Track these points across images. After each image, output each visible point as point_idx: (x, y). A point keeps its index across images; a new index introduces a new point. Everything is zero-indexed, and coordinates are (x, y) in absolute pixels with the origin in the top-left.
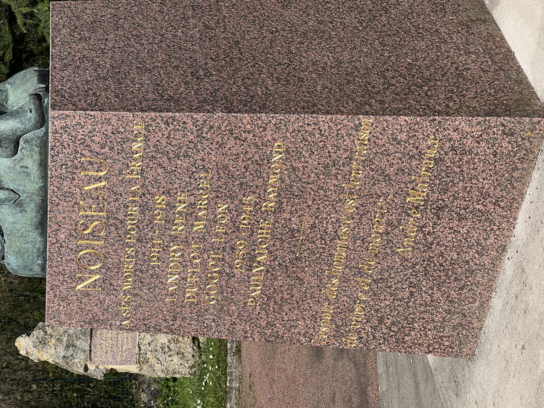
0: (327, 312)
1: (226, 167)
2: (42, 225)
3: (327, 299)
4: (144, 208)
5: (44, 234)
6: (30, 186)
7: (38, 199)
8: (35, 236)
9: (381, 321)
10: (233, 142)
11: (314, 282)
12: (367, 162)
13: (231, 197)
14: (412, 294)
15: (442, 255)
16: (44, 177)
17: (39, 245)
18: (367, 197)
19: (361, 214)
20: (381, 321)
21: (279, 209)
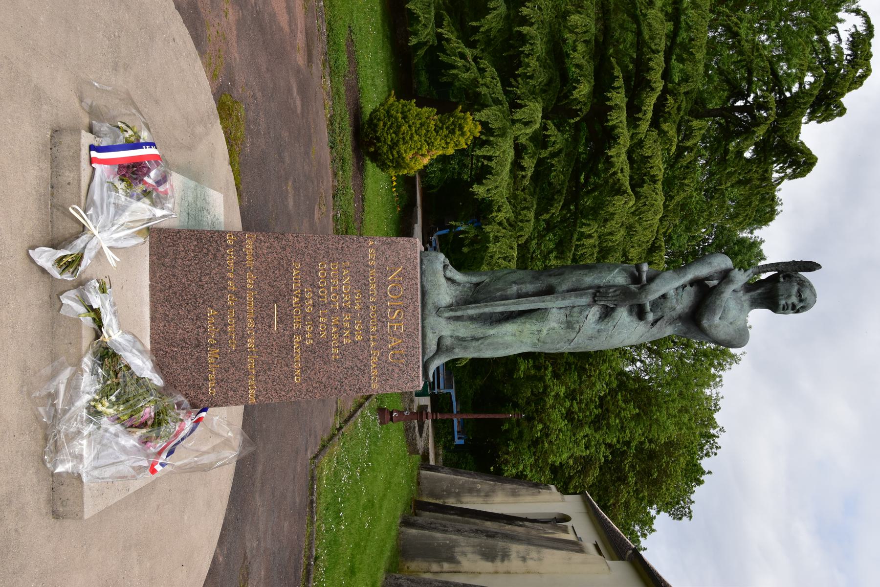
0: (250, 262)
1: (325, 363)
2: (424, 294)
3: (252, 271)
4: (367, 331)
5: (423, 287)
6: (432, 320)
7: (427, 312)
9: (215, 256)
10: (323, 380)
11: (262, 284)
12: (247, 374)
13: (319, 343)
14: (201, 280)
15: (189, 312)
16: (423, 327)
18: (242, 350)
19: (243, 338)
20: (215, 256)
21: (291, 337)
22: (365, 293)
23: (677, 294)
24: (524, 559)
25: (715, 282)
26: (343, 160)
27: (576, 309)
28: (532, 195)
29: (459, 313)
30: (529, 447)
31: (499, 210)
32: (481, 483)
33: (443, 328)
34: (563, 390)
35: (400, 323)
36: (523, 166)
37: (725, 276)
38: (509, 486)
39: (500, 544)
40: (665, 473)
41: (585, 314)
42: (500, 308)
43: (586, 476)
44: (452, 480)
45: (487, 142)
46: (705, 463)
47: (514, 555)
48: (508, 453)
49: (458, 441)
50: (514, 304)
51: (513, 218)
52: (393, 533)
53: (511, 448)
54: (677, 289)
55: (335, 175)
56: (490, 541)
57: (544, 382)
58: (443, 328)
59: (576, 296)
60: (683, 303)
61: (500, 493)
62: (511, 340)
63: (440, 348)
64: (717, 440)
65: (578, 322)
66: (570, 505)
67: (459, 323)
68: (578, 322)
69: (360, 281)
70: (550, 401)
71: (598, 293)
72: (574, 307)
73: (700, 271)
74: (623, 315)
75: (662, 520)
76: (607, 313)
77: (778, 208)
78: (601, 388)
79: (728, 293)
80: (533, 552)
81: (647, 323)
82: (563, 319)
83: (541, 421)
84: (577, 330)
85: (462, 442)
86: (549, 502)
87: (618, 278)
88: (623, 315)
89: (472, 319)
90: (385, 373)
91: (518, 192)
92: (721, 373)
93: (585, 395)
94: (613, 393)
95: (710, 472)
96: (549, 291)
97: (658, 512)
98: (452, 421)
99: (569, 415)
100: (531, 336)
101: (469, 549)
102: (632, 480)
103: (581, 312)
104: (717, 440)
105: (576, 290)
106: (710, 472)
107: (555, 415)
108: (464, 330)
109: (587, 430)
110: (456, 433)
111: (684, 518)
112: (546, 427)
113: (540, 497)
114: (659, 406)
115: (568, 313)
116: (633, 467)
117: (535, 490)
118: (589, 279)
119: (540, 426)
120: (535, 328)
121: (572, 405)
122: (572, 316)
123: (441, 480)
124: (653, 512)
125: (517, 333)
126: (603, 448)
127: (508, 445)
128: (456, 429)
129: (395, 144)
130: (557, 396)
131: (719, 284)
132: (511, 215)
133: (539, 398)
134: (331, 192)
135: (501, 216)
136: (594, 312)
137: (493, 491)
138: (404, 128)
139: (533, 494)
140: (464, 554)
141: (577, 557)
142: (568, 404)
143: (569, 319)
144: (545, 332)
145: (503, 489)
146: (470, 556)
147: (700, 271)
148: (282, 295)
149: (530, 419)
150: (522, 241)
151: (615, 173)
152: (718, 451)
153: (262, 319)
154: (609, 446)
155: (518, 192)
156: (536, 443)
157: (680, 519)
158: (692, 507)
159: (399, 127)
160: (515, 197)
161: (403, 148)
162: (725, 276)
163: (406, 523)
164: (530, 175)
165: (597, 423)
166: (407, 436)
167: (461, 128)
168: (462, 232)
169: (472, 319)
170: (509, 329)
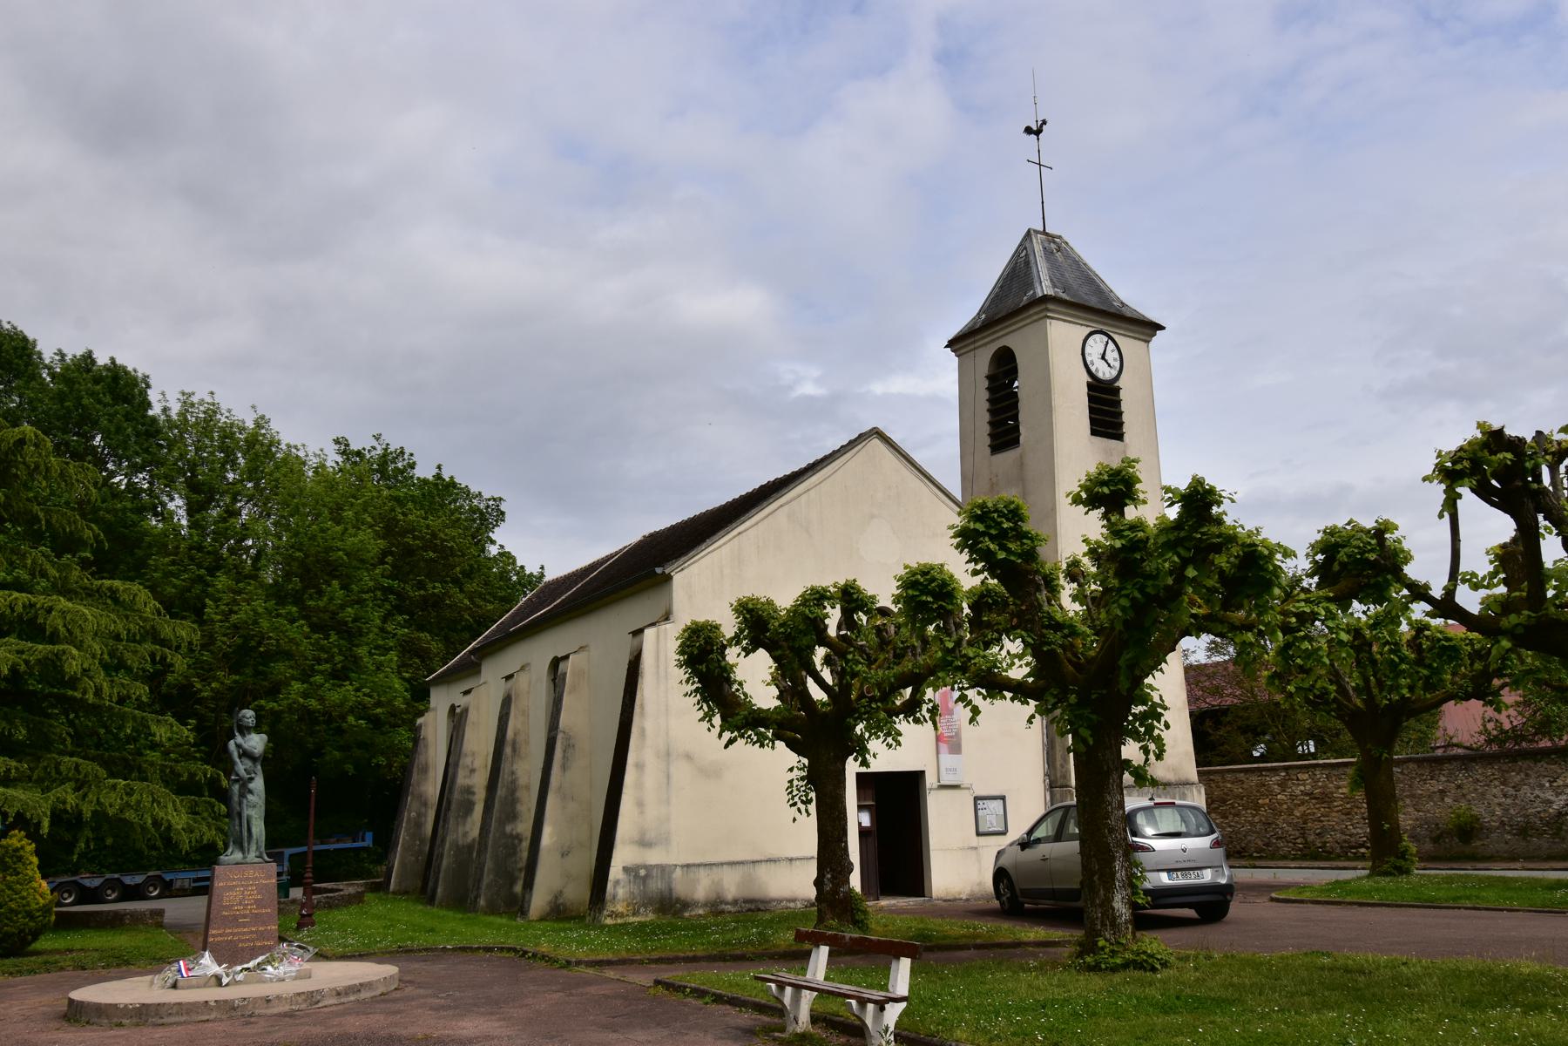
24: (473, 771)
26: (46, 963)
28: (39, 759)
30: (383, 734)
31: (64, 802)
32: (410, 811)
33: (252, 856)
34: (296, 686)
35: (250, 873)
37: (238, 746)
38: (415, 776)
39: (456, 796)
40: (432, 542)
42: (245, 834)
43: (427, 651)
44: (405, 849)
46: (424, 471)
47: (468, 782)
48: (390, 766)
49: (368, 842)
51: (72, 784)
52: (443, 912)
53: (382, 761)
55: (62, 969)
56: (453, 806)
57: (282, 712)
58: (252, 856)
60: (249, 763)
61: (423, 788)
62: (258, 828)
63: (260, 856)
64: (392, 449)
66: (441, 700)
69: (232, 888)
70: (313, 704)
71: (242, 795)
73: (235, 755)
74: (251, 786)
75: (503, 538)
76: (251, 792)
78: (298, 631)
79: (246, 746)
80: (466, 761)
83: (343, 717)
85: (369, 836)
86: (434, 725)
87: (236, 788)
88: (251, 786)
90: (269, 877)
91: (35, 777)
92: (283, 446)
93: (308, 654)
94: (306, 613)
95: (439, 467)
96: (240, 815)
97: (493, 542)
98: (315, 852)
99: (339, 676)
101: (461, 829)
102: (438, 588)
104: (392, 449)
105: (240, 804)
106: (439, 467)
107: (334, 697)
108: (253, 847)
109: (362, 651)
110: (355, 845)
111: (502, 508)
112: (351, 711)
113: (430, 738)
114: (329, 549)
116: (421, 585)
117: (421, 744)
118: (236, 799)
119: (351, 719)
121: (322, 672)
123: (402, 864)
124: (493, 550)
126: (390, 627)
127: (378, 765)
128: (349, 845)
129: (30, 915)
130: (305, 695)
132: (69, 786)
133: (307, 715)
134: (80, 972)
135: (71, 799)
136: (250, 797)
137: (421, 796)
138: (13, 905)
139: (426, 746)
140: (465, 834)
141: (472, 716)
142: (318, 679)
145: (419, 784)
146: (468, 828)
147: (235, 755)
148: (236, 918)
149: (340, 731)
150: (103, 773)
151: (27, 662)
152: (407, 451)
153: (244, 925)
154: (385, 619)
155: (35, 777)
156: (376, 722)
157: (503, 513)
158: (486, 495)
159: (11, 910)
160: (40, 781)
161: (34, 906)
162: (238, 746)
163: (431, 900)
164: (14, 764)
165: (351, 634)
166: (337, 906)
167: (17, 850)
168: (88, 846)
170: (254, 830)
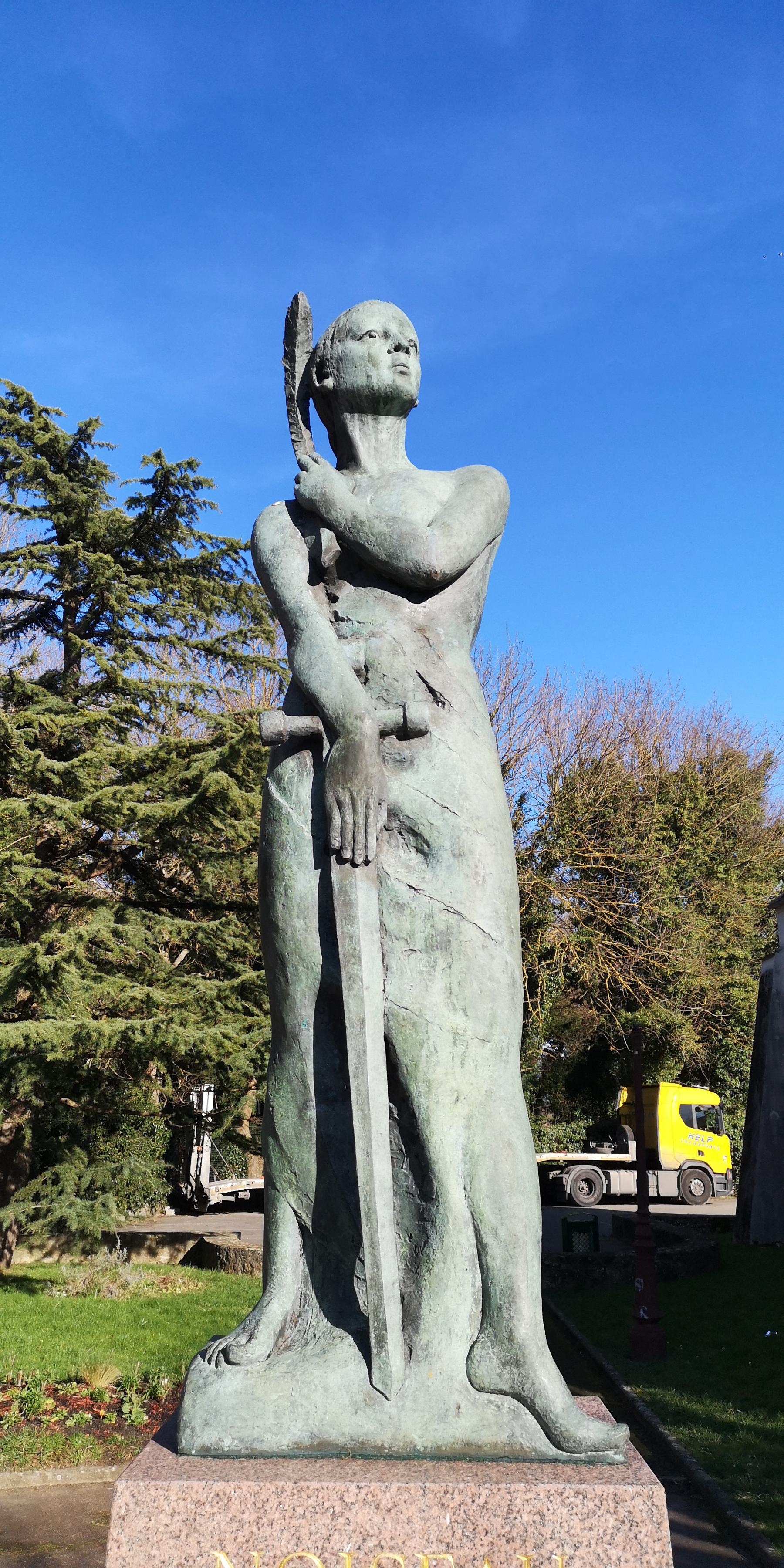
8: (292, 1432)
17: (272, 1442)
22: (596, 893)
23: (356, 635)
25: (327, 536)
27: (392, 924)
29: (393, 1314)
36: (86, 818)
41: (405, 895)
45: (200, 506)
50: (366, 1118)
54: (341, 637)
59: (351, 919)
65: (431, 916)
67: (425, 1311)
68: (431, 916)
72: (383, 926)
77: (49, 638)
81: (435, 719)
82: (418, 961)
84: (453, 919)
89: (417, 1259)
100: (470, 1064)
103: (400, 907)
115: (401, 946)
120: (445, 1050)
122: (411, 935)
125: (462, 1109)
131: (331, 526)
143: (419, 944)
144: (459, 1020)
169: (417, 1259)
